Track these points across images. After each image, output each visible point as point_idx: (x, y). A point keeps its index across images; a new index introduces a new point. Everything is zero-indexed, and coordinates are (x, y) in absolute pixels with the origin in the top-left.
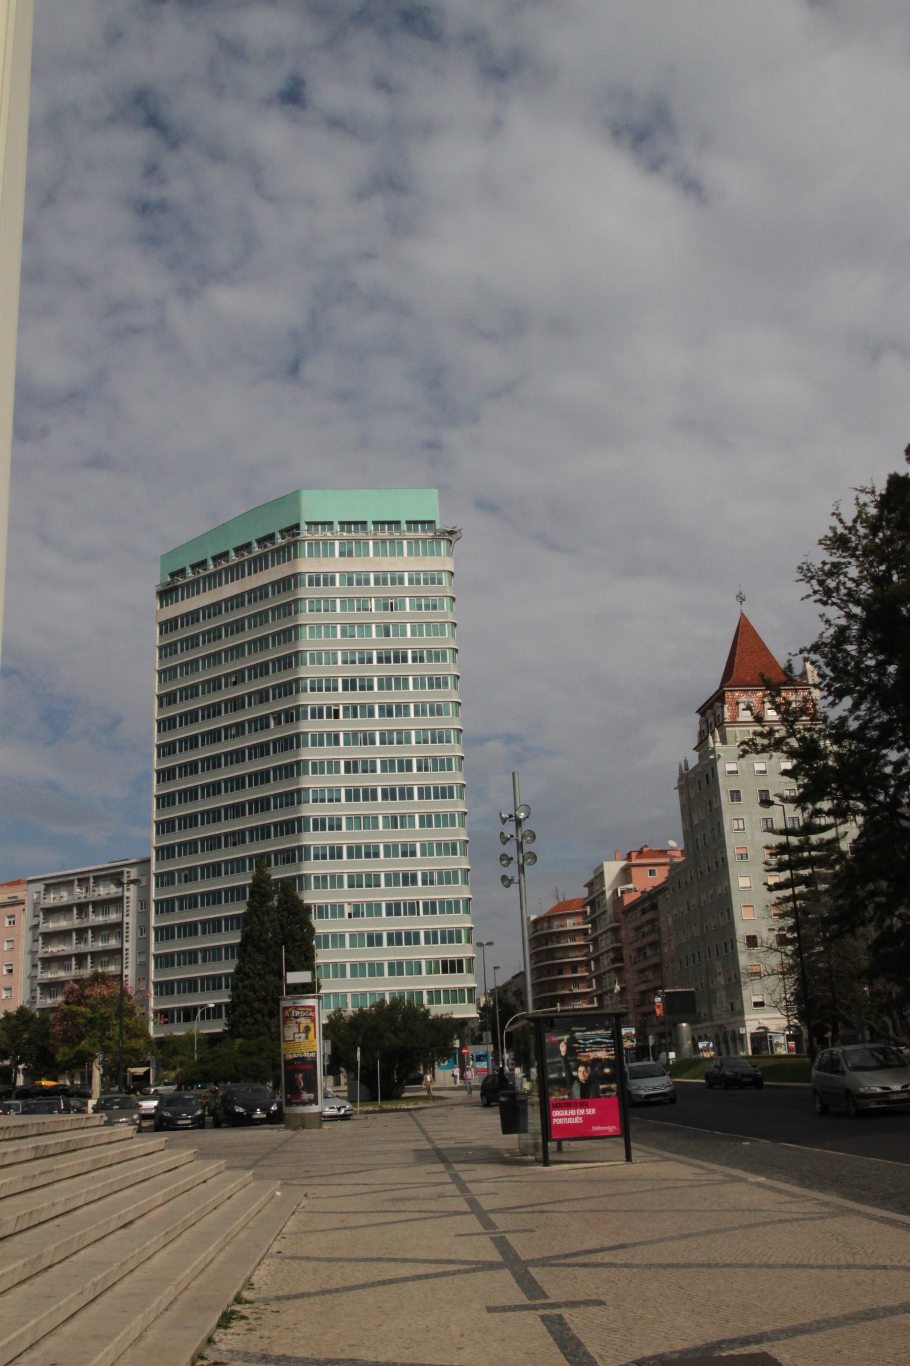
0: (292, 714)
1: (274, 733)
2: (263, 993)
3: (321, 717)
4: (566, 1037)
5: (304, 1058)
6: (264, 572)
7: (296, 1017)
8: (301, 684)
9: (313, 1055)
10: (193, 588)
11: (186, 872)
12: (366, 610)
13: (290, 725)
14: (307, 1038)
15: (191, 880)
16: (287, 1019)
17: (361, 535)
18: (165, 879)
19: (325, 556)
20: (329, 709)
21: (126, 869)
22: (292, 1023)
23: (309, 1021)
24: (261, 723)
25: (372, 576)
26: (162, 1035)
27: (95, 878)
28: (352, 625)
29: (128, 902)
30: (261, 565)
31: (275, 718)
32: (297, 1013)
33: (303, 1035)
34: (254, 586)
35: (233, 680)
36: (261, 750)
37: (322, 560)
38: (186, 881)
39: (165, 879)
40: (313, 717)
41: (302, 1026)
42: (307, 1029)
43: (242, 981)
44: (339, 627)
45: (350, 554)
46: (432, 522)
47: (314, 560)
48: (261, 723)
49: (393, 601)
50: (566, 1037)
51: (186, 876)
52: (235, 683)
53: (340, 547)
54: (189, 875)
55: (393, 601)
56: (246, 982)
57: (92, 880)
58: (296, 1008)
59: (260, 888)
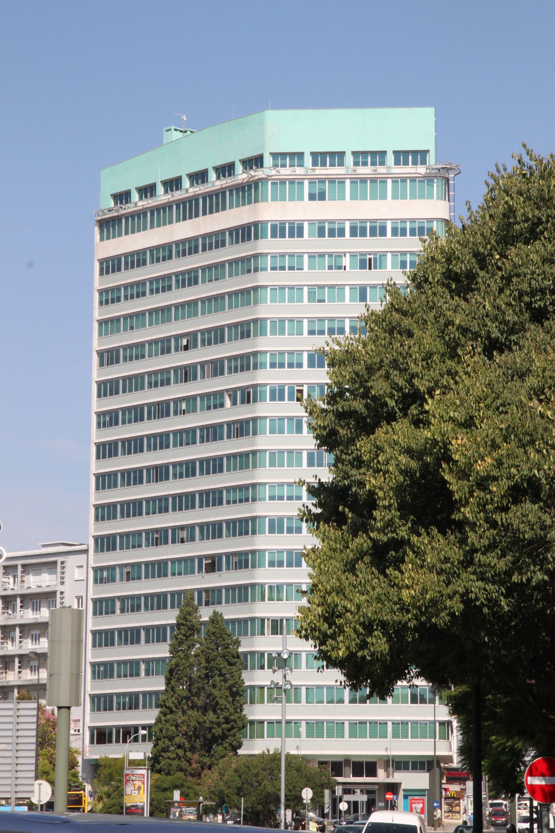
0: (249, 393)
1: (230, 413)
2: (185, 728)
3: (282, 399)
4: (179, 810)
5: (137, 806)
6: (221, 214)
7: (133, 781)
8: (260, 358)
9: (142, 804)
10: (138, 220)
11: (129, 569)
12: (339, 268)
13: (246, 407)
14: (139, 793)
15: (133, 579)
16: (128, 781)
17: (336, 171)
18: (105, 574)
19: (292, 199)
20: (291, 389)
21: (59, 559)
22: (130, 784)
23: (141, 783)
24: (214, 401)
25: (347, 226)
26: (97, 757)
27: (23, 566)
28: (321, 287)
29: (62, 598)
30: (217, 203)
31: (230, 396)
32: (134, 778)
33: (137, 792)
34: (209, 230)
35: (185, 342)
36: (212, 433)
37: (288, 204)
38: (128, 580)
39: (105, 574)
40: (273, 398)
41: (136, 787)
42: (139, 788)
43: (165, 715)
44: (306, 289)
45: (322, 197)
46: (424, 153)
47: (278, 204)
48: (214, 401)
49: (372, 256)
50: (179, 810)
51: (128, 573)
52: (186, 348)
53: (310, 188)
54: (132, 573)
55: (372, 256)
56: (169, 717)
57: (20, 569)
58: (133, 775)
59: (186, 620)
